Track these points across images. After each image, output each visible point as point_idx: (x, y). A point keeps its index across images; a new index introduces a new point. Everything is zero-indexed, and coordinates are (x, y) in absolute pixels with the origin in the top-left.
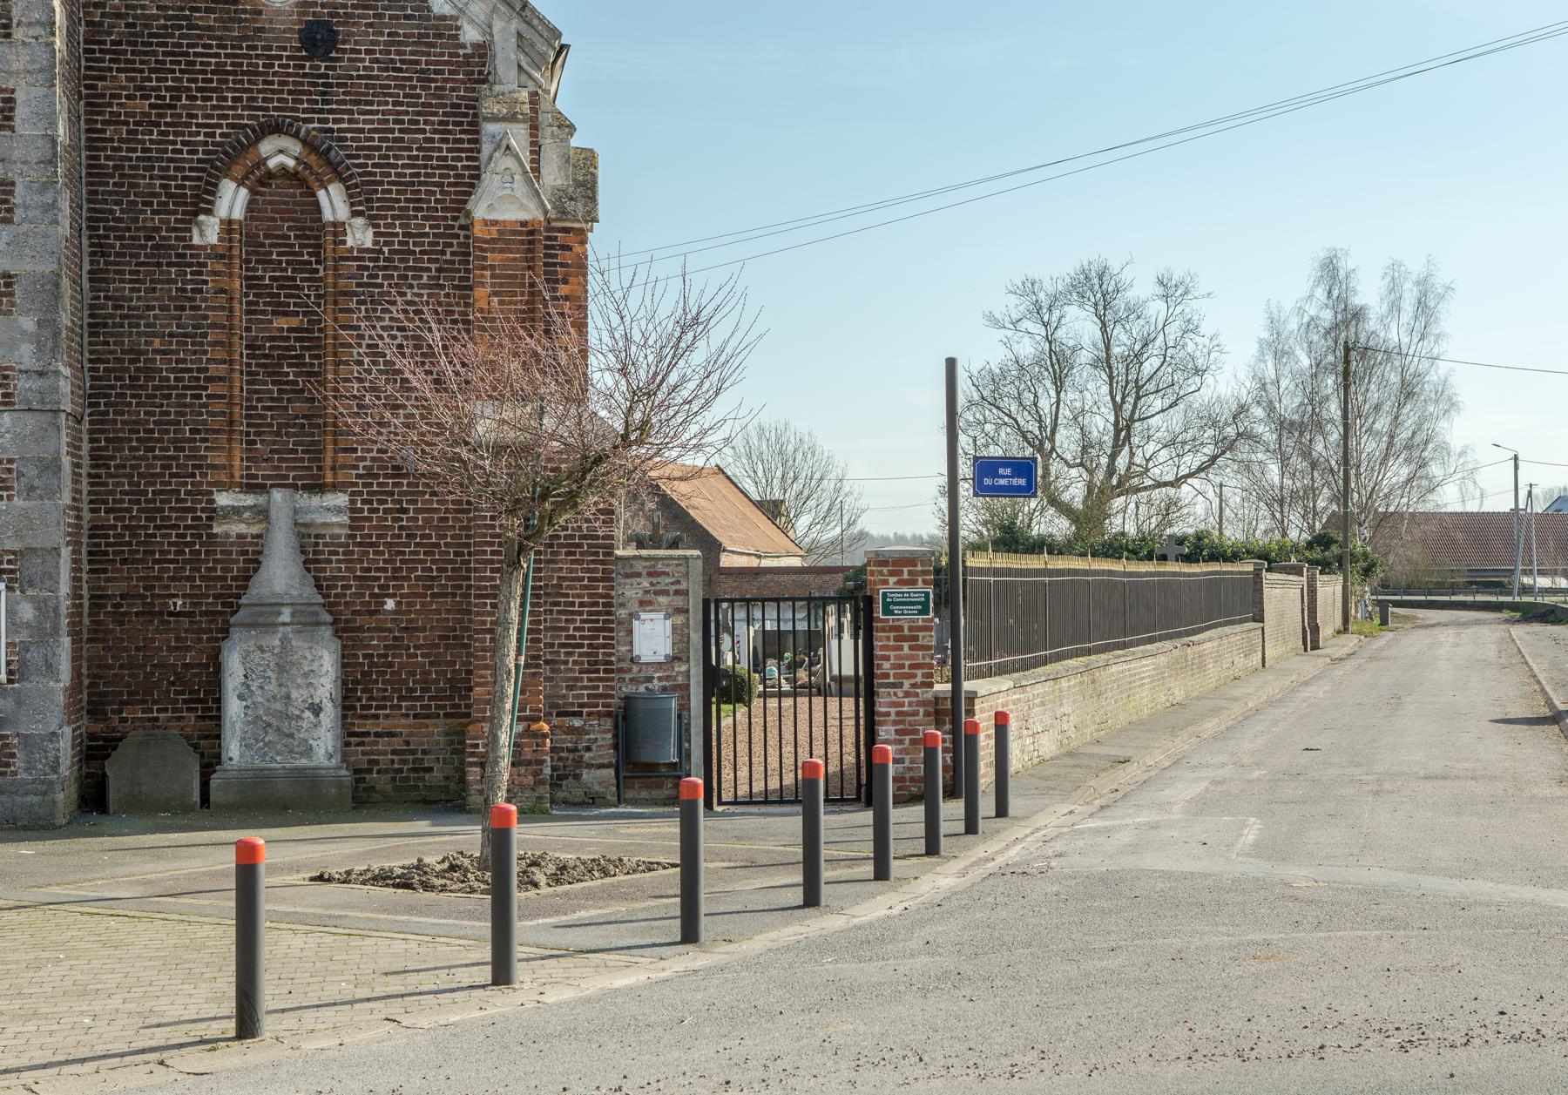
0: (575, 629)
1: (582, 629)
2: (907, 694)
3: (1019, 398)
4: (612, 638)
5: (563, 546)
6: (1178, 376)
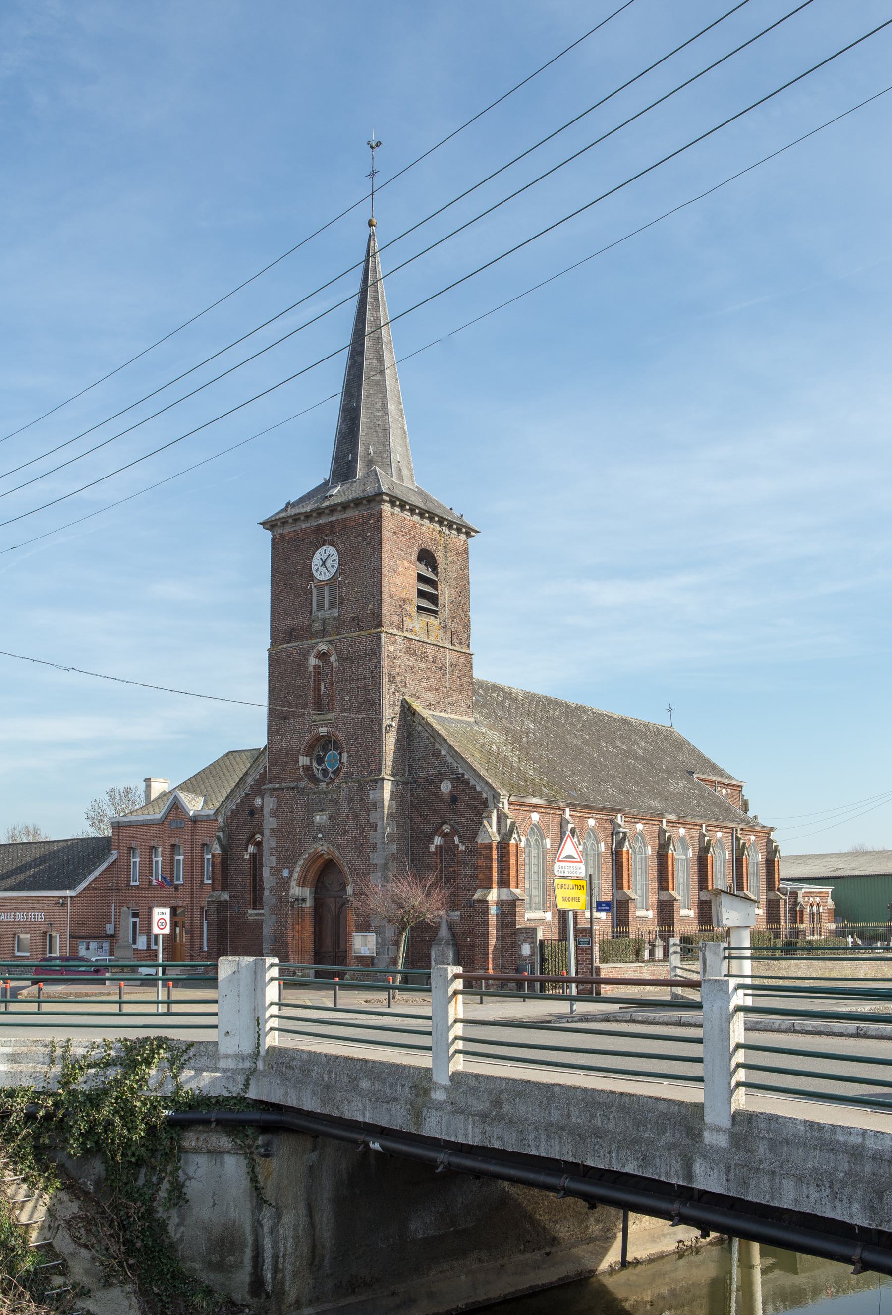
2: (585, 967)
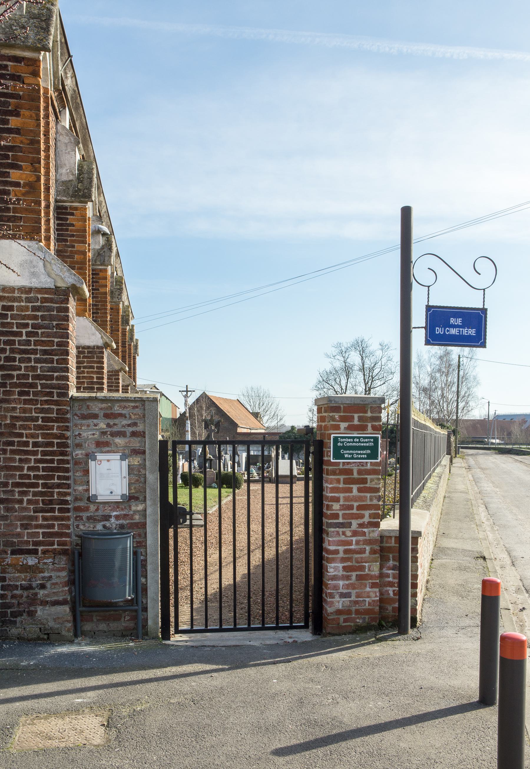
0: (30, 469)
1: (37, 469)
2: (355, 533)
3: (335, 380)
4: (68, 478)
5: (15, 385)
6: (385, 375)
